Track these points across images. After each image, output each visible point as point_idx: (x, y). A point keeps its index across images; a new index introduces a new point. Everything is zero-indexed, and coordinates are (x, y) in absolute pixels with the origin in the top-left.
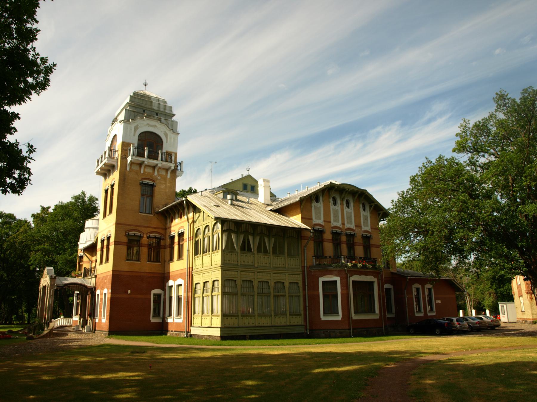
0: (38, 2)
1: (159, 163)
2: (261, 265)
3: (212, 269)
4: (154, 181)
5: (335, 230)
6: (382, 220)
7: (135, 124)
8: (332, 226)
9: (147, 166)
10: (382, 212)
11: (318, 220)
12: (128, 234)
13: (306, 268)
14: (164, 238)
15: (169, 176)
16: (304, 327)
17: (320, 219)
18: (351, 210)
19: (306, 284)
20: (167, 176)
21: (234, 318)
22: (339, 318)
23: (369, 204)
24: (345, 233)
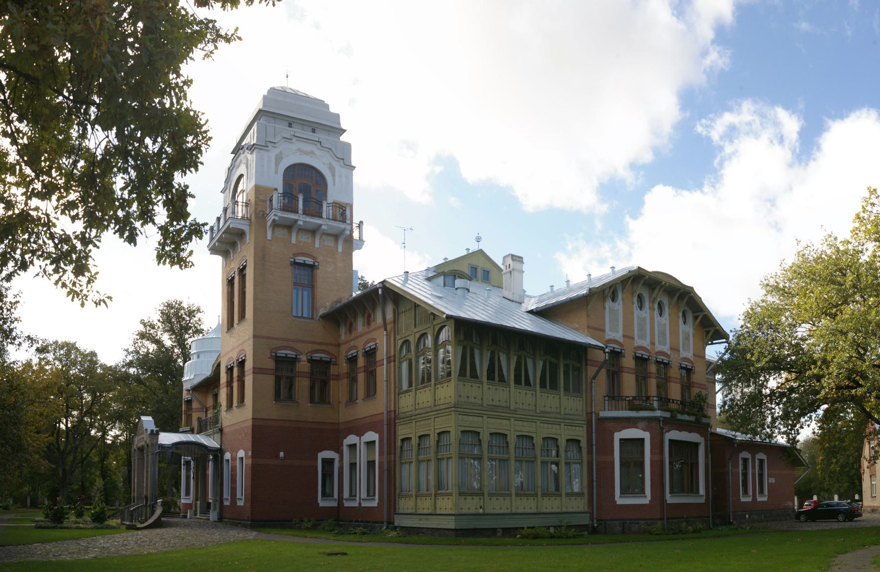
0: (150, 222)
1: (325, 223)
2: (521, 407)
3: (436, 412)
4: (315, 258)
5: (640, 353)
6: (710, 342)
7: (277, 151)
8: (636, 345)
9: (301, 230)
11: (614, 333)
12: (276, 354)
13: (594, 415)
14: (336, 362)
17: (617, 332)
18: (665, 320)
20: (337, 248)
21: (476, 499)
22: (646, 500)
23: (693, 312)
24: (655, 359)
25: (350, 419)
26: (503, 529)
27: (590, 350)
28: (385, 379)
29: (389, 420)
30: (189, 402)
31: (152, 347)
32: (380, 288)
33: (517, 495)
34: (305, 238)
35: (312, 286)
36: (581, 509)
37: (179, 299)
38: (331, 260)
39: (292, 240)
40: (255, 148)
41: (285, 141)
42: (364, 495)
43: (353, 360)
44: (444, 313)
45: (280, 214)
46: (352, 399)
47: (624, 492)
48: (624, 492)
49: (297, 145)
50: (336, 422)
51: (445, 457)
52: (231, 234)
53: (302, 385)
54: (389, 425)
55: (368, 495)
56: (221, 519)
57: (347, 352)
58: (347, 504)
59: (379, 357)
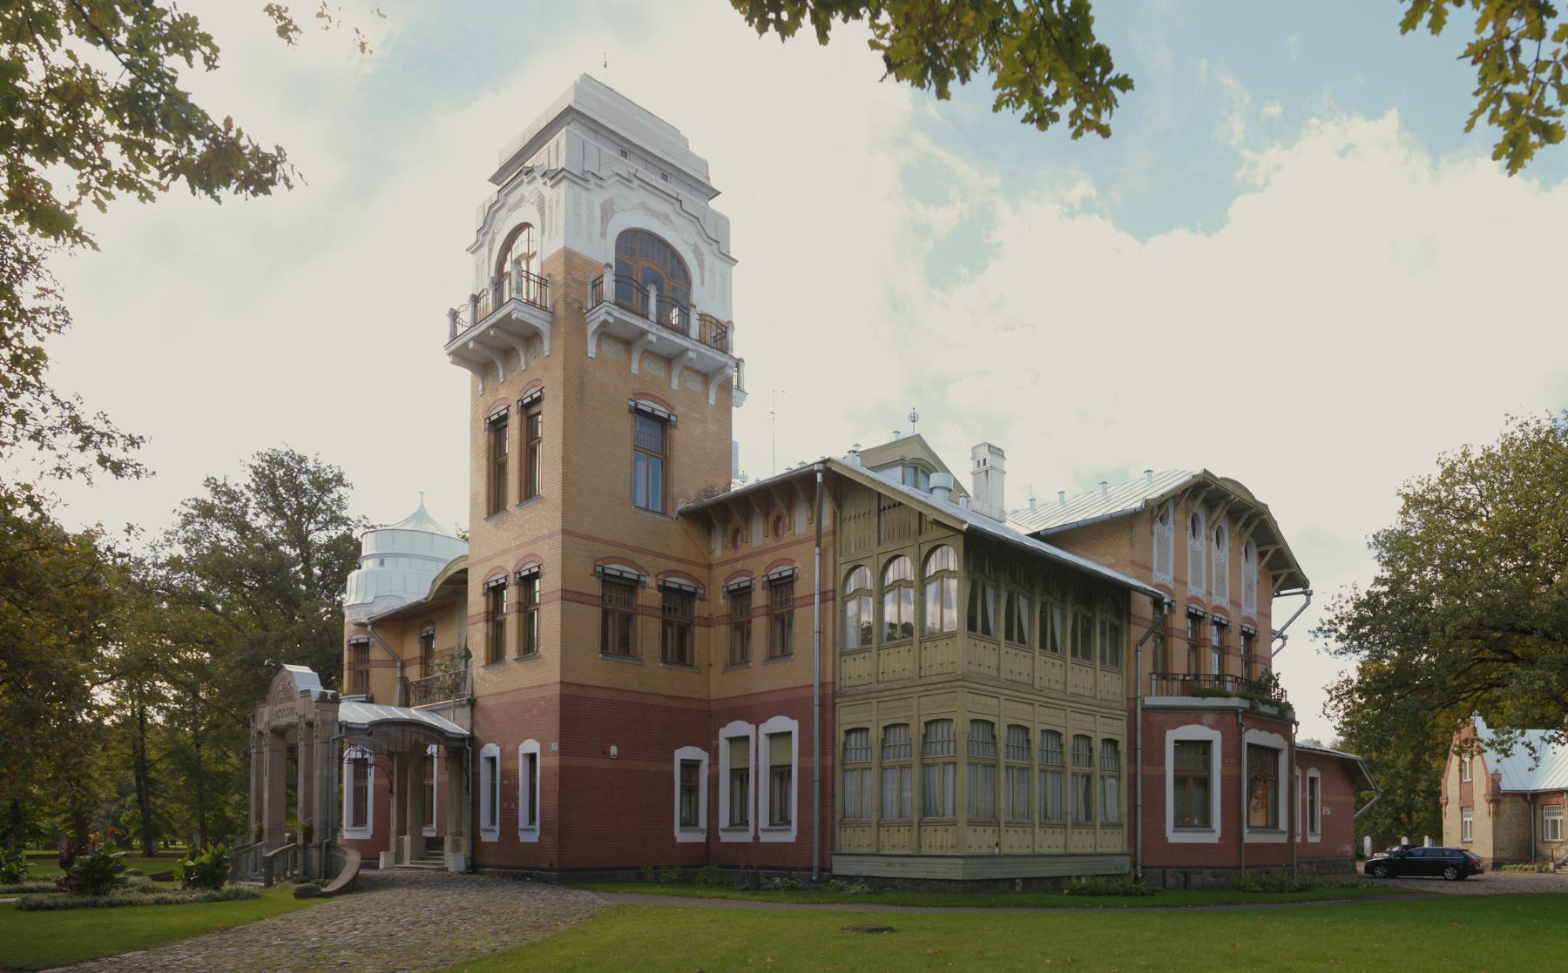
3: (925, 687)
4: (670, 408)
8: (1189, 594)
10: (1285, 573)
12: (603, 570)
14: (704, 594)
15: (712, 401)
16: (1128, 858)
19: (1139, 747)
21: (989, 830)
22: (1213, 837)
23: (1258, 546)
25: (735, 695)
26: (1023, 879)
27: (1135, 595)
28: (816, 629)
29: (823, 698)
30: (361, 648)
31: (228, 536)
32: (818, 471)
33: (1042, 825)
34: (654, 369)
35: (663, 458)
36: (1118, 850)
37: (298, 452)
38: (697, 416)
39: (633, 366)
40: (564, 177)
41: (618, 181)
42: (764, 822)
43: (740, 595)
44: (964, 522)
45: (617, 312)
46: (739, 658)
47: (1180, 824)
48: (1180, 824)
49: (638, 195)
50: (704, 697)
51: (940, 761)
52: (508, 332)
53: (648, 631)
54: (822, 705)
55: (771, 824)
56: (474, 866)
57: (728, 579)
58: (725, 838)
59: (800, 590)
